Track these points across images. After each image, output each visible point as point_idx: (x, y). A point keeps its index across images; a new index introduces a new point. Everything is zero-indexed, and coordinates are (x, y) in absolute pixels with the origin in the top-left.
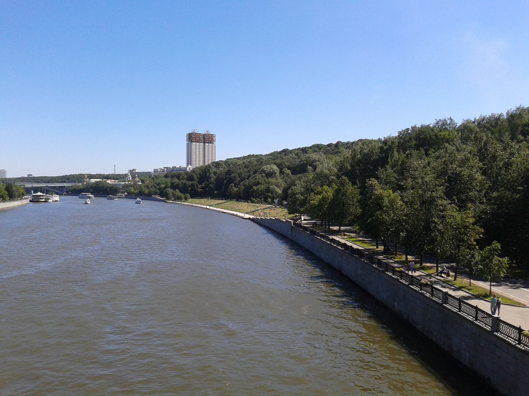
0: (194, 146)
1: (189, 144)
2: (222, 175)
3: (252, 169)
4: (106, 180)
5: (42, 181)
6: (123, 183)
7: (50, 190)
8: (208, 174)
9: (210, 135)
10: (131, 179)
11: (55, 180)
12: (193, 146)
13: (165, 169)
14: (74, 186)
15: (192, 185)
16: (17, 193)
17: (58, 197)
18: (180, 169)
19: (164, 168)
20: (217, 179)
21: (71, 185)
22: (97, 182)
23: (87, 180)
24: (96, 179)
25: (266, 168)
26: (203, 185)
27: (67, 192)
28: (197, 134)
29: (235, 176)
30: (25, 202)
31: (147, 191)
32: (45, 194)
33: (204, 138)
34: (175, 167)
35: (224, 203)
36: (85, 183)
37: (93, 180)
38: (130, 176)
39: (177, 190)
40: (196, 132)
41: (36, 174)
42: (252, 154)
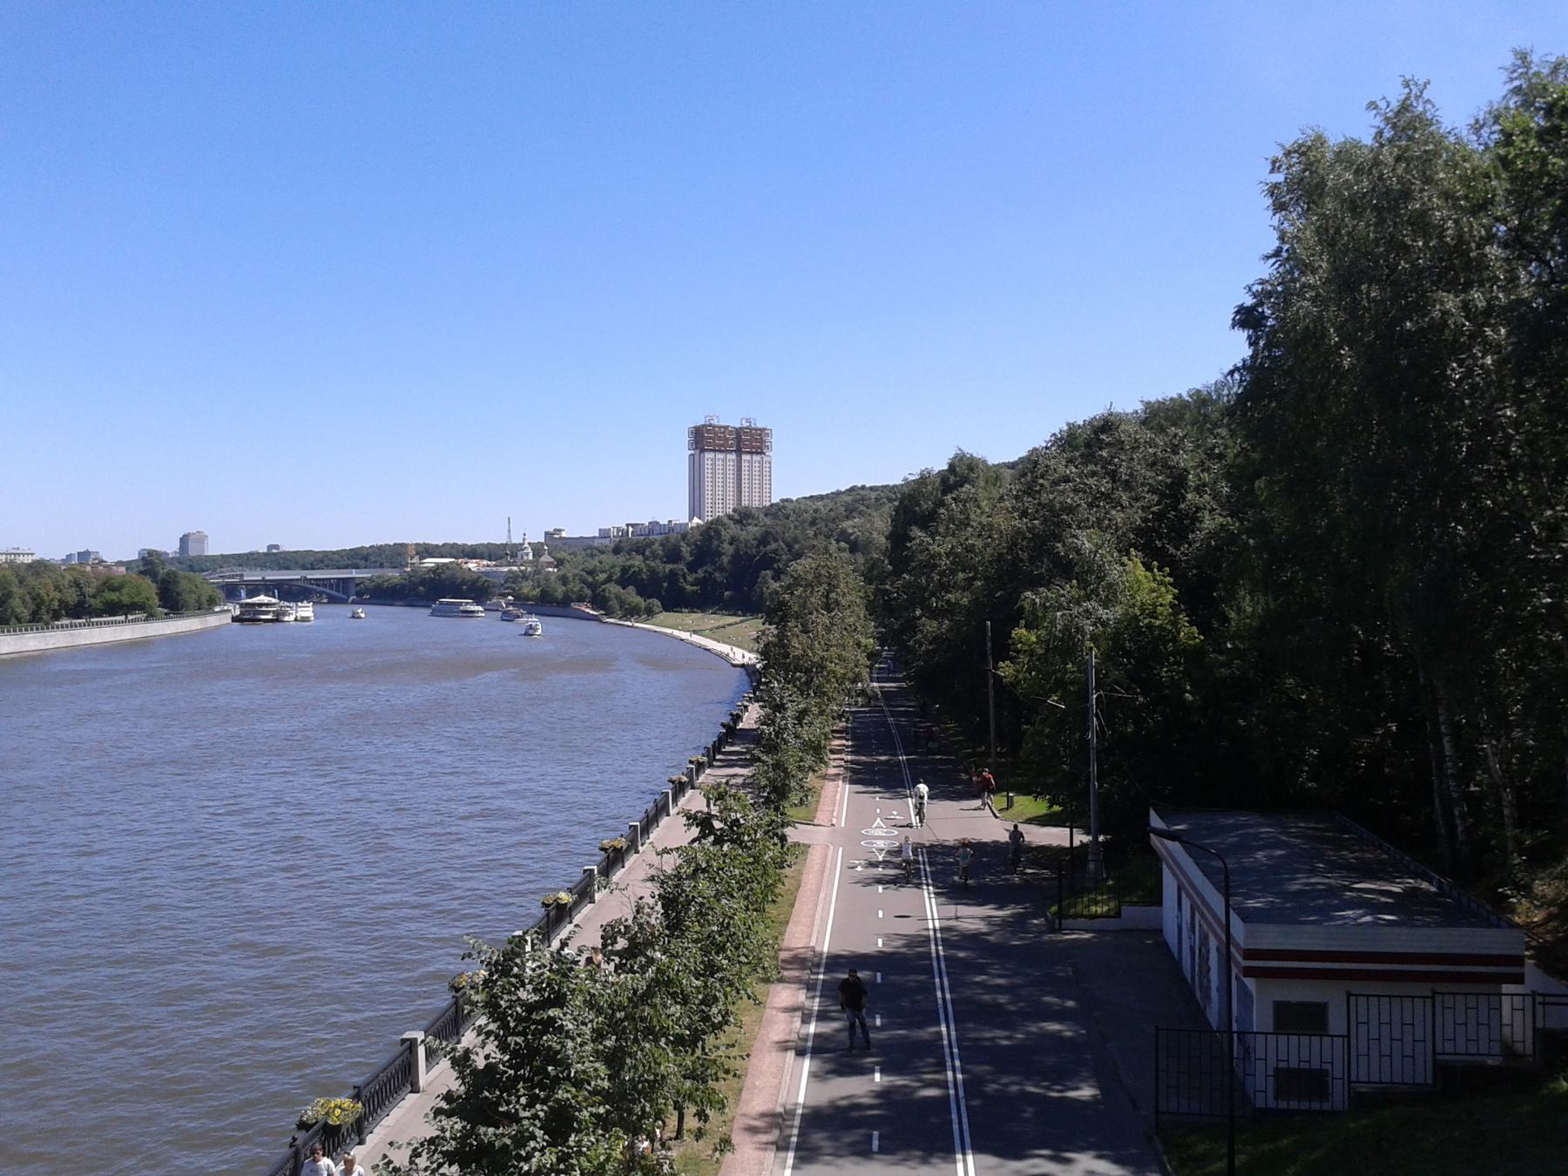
0: (710, 462)
1: (697, 457)
2: (749, 545)
3: (824, 529)
4: (466, 560)
5: (297, 563)
6: (506, 569)
7: (315, 590)
8: (716, 543)
9: (756, 429)
10: (531, 557)
11: (331, 560)
12: (708, 464)
13: (631, 529)
14: (379, 577)
15: (673, 573)
16: (191, 599)
17: (311, 609)
18: (670, 528)
19: (628, 525)
20: (736, 557)
21: (370, 575)
22: (438, 566)
23: (414, 561)
24: (442, 557)
25: (854, 527)
26: (700, 573)
27: (359, 594)
28: (720, 427)
29: (777, 550)
30: (212, 621)
31: (560, 591)
32: (274, 600)
33: (739, 439)
34: (657, 523)
35: (736, 623)
36: (409, 569)
37: (430, 562)
38: (530, 550)
39: (631, 589)
40: (715, 422)
41: (289, 545)
42: (860, 485)
